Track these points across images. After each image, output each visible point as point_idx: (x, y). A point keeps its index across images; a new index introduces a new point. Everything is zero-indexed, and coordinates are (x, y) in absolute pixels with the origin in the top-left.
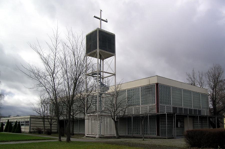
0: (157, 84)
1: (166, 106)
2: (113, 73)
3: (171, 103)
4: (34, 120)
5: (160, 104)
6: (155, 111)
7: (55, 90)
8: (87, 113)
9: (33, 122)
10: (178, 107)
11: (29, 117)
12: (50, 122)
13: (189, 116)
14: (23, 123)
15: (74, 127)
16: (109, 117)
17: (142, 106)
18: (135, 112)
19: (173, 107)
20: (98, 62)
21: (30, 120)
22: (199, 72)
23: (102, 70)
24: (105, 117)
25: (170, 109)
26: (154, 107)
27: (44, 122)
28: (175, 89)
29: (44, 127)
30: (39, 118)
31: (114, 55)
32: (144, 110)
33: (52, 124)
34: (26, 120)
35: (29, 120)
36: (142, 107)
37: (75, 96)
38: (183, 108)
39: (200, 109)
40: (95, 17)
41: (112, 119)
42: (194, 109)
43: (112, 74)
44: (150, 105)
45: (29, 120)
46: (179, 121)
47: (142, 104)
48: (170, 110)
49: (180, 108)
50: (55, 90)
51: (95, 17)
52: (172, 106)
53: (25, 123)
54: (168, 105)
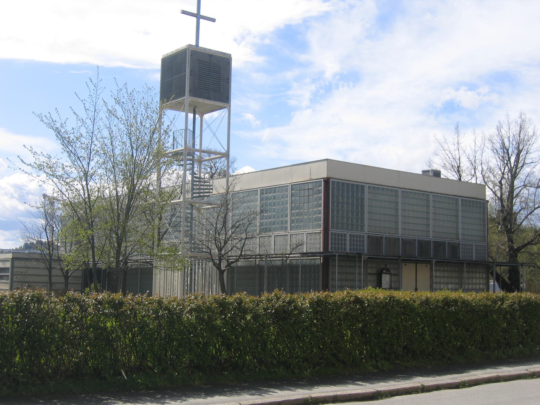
0: (327, 181)
2: (223, 151)
4: (23, 266)
5: (331, 231)
6: (320, 248)
7: (90, 207)
9: (20, 270)
11: (10, 256)
20: (186, 129)
23: (197, 147)
27: (50, 269)
28: (376, 189)
29: (304, 190)
30: (37, 260)
31: (226, 108)
33: (69, 277)
35: (8, 265)
37: (79, 311)
38: (401, 238)
39: (457, 241)
42: (434, 242)
43: (220, 154)
45: (8, 265)
50: (90, 207)
54: (355, 233)
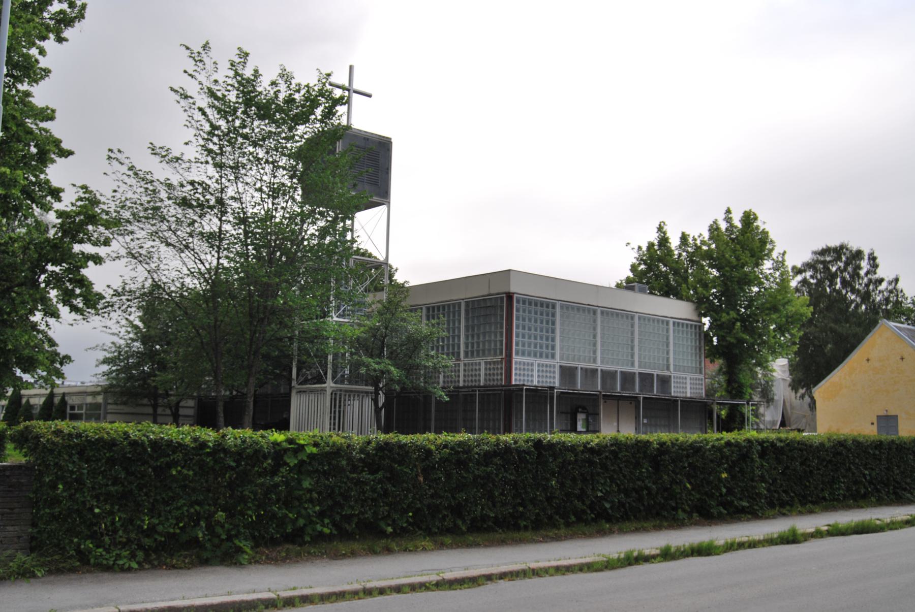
1: (539, 365)
3: (596, 357)
5: (516, 358)
8: (333, 378)
10: (619, 370)
12: (173, 409)
13: (604, 395)
14: (76, 411)
15: (620, 412)
16: (358, 396)
17: (467, 361)
18: (541, 380)
19: (561, 367)
21: (105, 399)
22: (161, 162)
24: (345, 395)
25: (520, 375)
26: (499, 367)
32: (472, 375)
34: (89, 400)
36: (465, 365)
39: (666, 373)
40: (351, 68)
41: (372, 399)
44: (489, 359)
46: (580, 410)
47: (466, 355)
48: (552, 375)
49: (586, 370)
51: (351, 68)
52: (557, 362)
53: (83, 412)
